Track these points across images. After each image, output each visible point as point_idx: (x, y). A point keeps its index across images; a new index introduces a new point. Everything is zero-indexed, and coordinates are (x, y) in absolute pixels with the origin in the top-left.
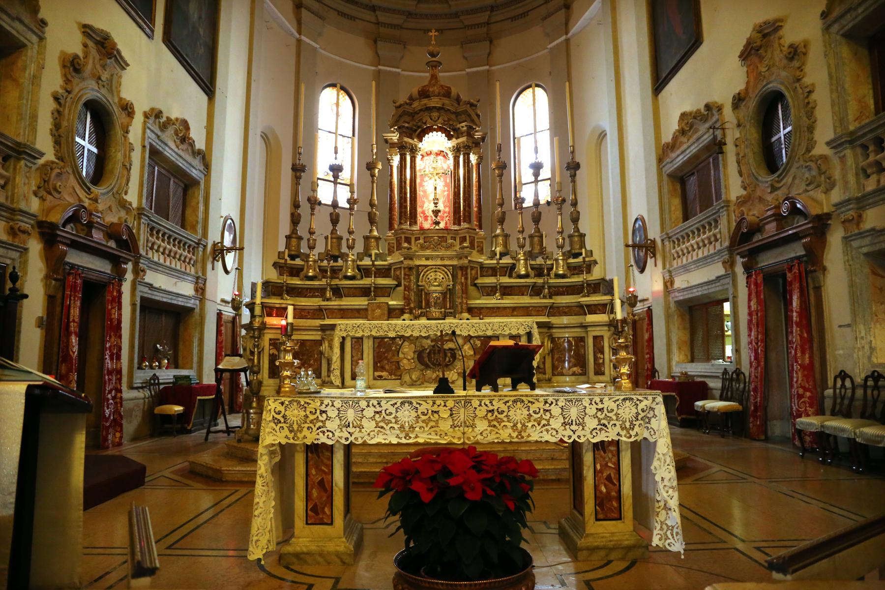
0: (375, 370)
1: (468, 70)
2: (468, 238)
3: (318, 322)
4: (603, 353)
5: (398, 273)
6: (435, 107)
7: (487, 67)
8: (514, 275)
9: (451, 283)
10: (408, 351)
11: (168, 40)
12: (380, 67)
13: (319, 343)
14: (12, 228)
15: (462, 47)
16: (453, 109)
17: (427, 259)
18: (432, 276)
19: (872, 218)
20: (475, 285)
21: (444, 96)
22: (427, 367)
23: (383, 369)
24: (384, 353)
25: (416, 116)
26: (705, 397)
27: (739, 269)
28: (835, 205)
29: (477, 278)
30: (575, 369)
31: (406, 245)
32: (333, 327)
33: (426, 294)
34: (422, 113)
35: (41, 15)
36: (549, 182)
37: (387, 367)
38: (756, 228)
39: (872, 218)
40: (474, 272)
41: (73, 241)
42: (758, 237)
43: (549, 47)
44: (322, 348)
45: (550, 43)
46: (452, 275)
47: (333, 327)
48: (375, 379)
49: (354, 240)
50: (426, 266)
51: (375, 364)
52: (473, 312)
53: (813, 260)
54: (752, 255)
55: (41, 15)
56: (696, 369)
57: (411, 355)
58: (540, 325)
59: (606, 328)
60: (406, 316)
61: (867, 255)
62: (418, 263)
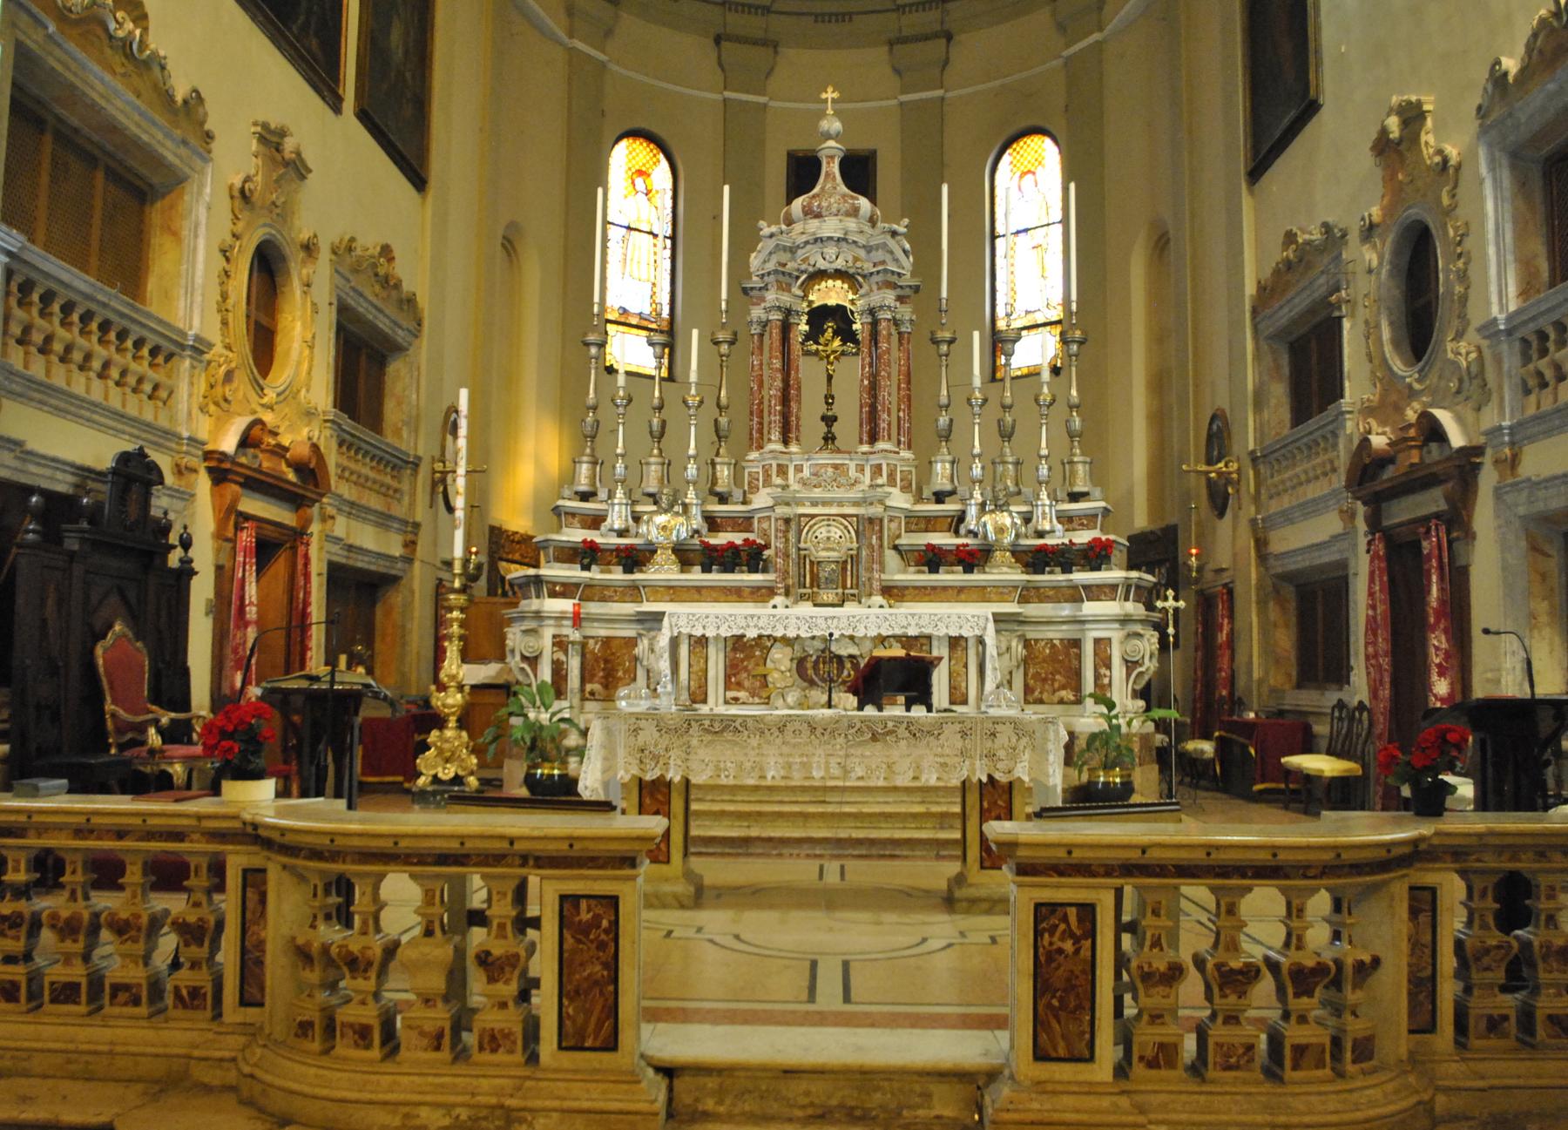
0: (727, 688)
1: (904, 98)
2: (884, 467)
3: (629, 608)
4: (1109, 667)
5: (765, 525)
6: (830, 238)
7: (939, 93)
8: (962, 530)
9: (855, 545)
10: (780, 659)
11: (363, 116)
12: (727, 94)
13: (632, 642)
14: (177, 465)
15: (891, 50)
16: (862, 240)
17: (814, 504)
18: (822, 532)
19: (1539, 460)
20: (896, 548)
21: (848, 214)
22: (812, 683)
23: (739, 686)
24: (742, 661)
25: (800, 252)
26: (1308, 748)
27: (1361, 526)
28: (1487, 433)
29: (899, 536)
30: (1063, 693)
31: (779, 481)
32: (658, 617)
33: (812, 563)
34: (809, 247)
35: (207, 127)
36: (1057, 330)
37: (746, 684)
38: (1384, 461)
39: (1539, 460)
40: (894, 525)
41: (247, 477)
42: (1389, 472)
43: (1065, 53)
44: (637, 651)
45: (1068, 46)
46: (857, 532)
47: (658, 617)
48: (726, 702)
49: (664, 424)
50: (813, 516)
51: (727, 677)
52: (893, 593)
53: (1457, 520)
54: (1376, 503)
55: (207, 127)
56: (1308, 699)
57: (786, 664)
58: (999, 619)
59: (1117, 626)
60: (779, 600)
61: (1523, 518)
62: (801, 510)
